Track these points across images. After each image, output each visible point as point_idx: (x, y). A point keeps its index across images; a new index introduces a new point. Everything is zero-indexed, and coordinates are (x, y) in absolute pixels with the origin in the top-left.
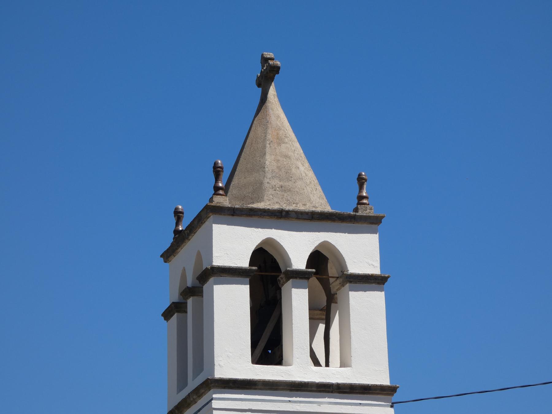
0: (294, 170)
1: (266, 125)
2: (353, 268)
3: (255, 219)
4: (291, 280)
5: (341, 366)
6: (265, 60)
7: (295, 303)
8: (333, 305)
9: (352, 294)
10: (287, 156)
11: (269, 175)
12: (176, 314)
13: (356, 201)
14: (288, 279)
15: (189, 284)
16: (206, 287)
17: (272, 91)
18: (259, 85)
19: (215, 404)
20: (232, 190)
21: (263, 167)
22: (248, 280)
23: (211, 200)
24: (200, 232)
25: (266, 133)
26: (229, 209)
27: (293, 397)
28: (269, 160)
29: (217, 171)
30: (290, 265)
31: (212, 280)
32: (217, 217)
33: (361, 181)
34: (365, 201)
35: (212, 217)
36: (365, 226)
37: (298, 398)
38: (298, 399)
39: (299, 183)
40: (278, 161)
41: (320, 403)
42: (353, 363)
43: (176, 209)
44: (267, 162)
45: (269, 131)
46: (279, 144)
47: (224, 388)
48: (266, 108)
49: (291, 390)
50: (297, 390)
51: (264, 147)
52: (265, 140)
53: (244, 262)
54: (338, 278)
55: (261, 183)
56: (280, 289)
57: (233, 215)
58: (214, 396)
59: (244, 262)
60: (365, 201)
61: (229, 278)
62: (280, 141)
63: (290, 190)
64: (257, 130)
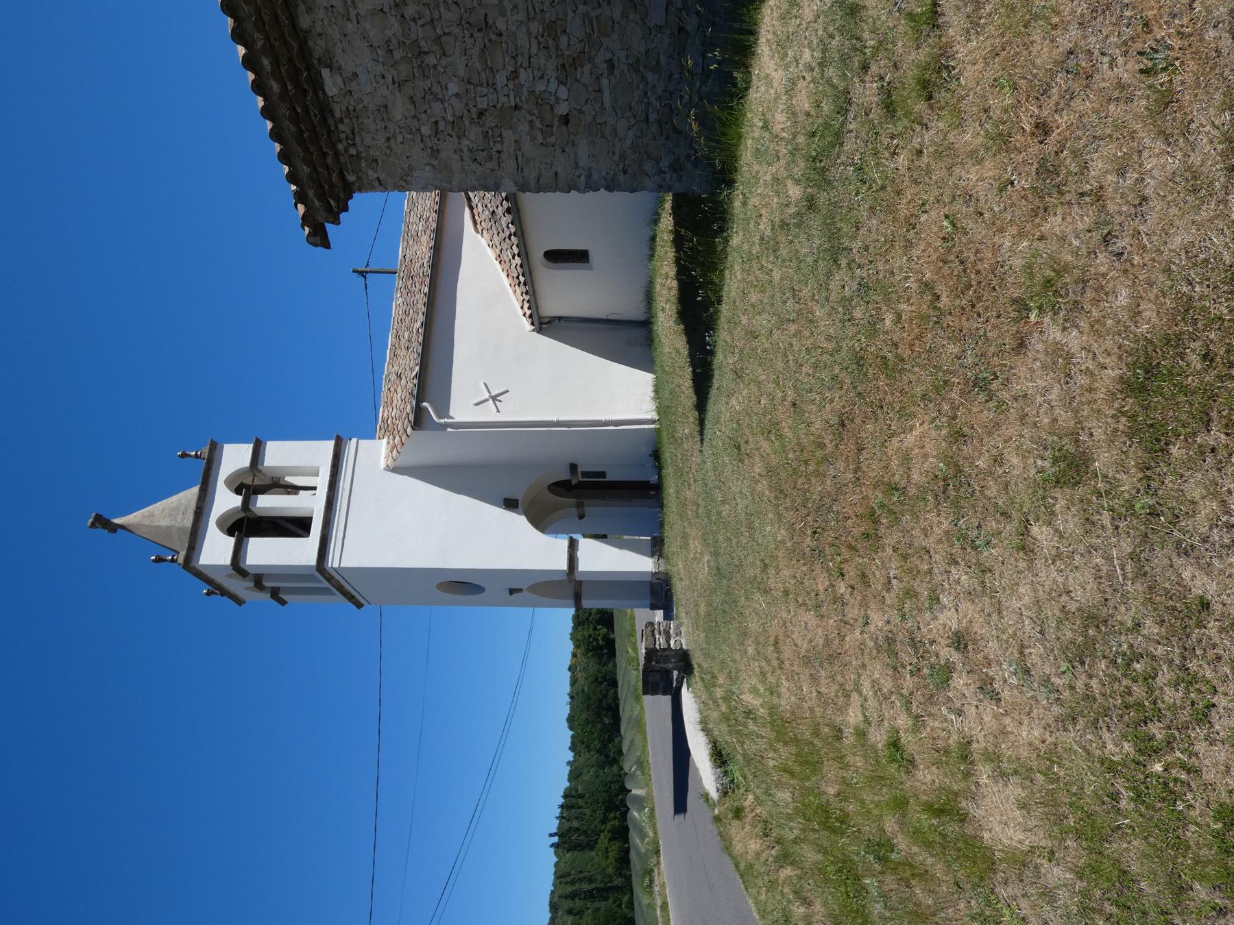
0: (173, 505)
1: (139, 526)
2: (246, 462)
3: (200, 532)
4: (250, 507)
5: (318, 476)
6: (93, 525)
7: (267, 505)
8: (281, 483)
9: (266, 464)
10: (163, 510)
11: (174, 523)
12: (280, 596)
13: (199, 460)
14: (250, 510)
15: (252, 584)
16: (251, 571)
17: (117, 521)
18: (115, 531)
19: (336, 565)
20: (177, 549)
21: (168, 527)
22: (245, 539)
23: (180, 564)
24: (210, 574)
25: (145, 525)
26: (188, 551)
27: (573, 748)
28: (163, 523)
29: (159, 560)
30: (238, 507)
31: (242, 566)
32: (194, 558)
33: (184, 455)
34: (199, 453)
35: (193, 564)
36: (217, 452)
37: (570, 756)
38: (338, 505)
39: (182, 502)
40: (165, 516)
41: (343, 489)
42: (315, 464)
43: (205, 594)
44: (165, 524)
45: (143, 523)
46: (153, 516)
47: (324, 558)
48: (129, 525)
49: (331, 509)
50: (332, 505)
51: (155, 527)
52: (149, 526)
53: (232, 540)
54: (254, 475)
55: (179, 529)
56: (261, 518)
57: (194, 549)
58: (330, 565)
59: (232, 540)
60: (199, 453)
61: (242, 553)
62: (151, 515)
63: (186, 508)
64: (142, 532)
